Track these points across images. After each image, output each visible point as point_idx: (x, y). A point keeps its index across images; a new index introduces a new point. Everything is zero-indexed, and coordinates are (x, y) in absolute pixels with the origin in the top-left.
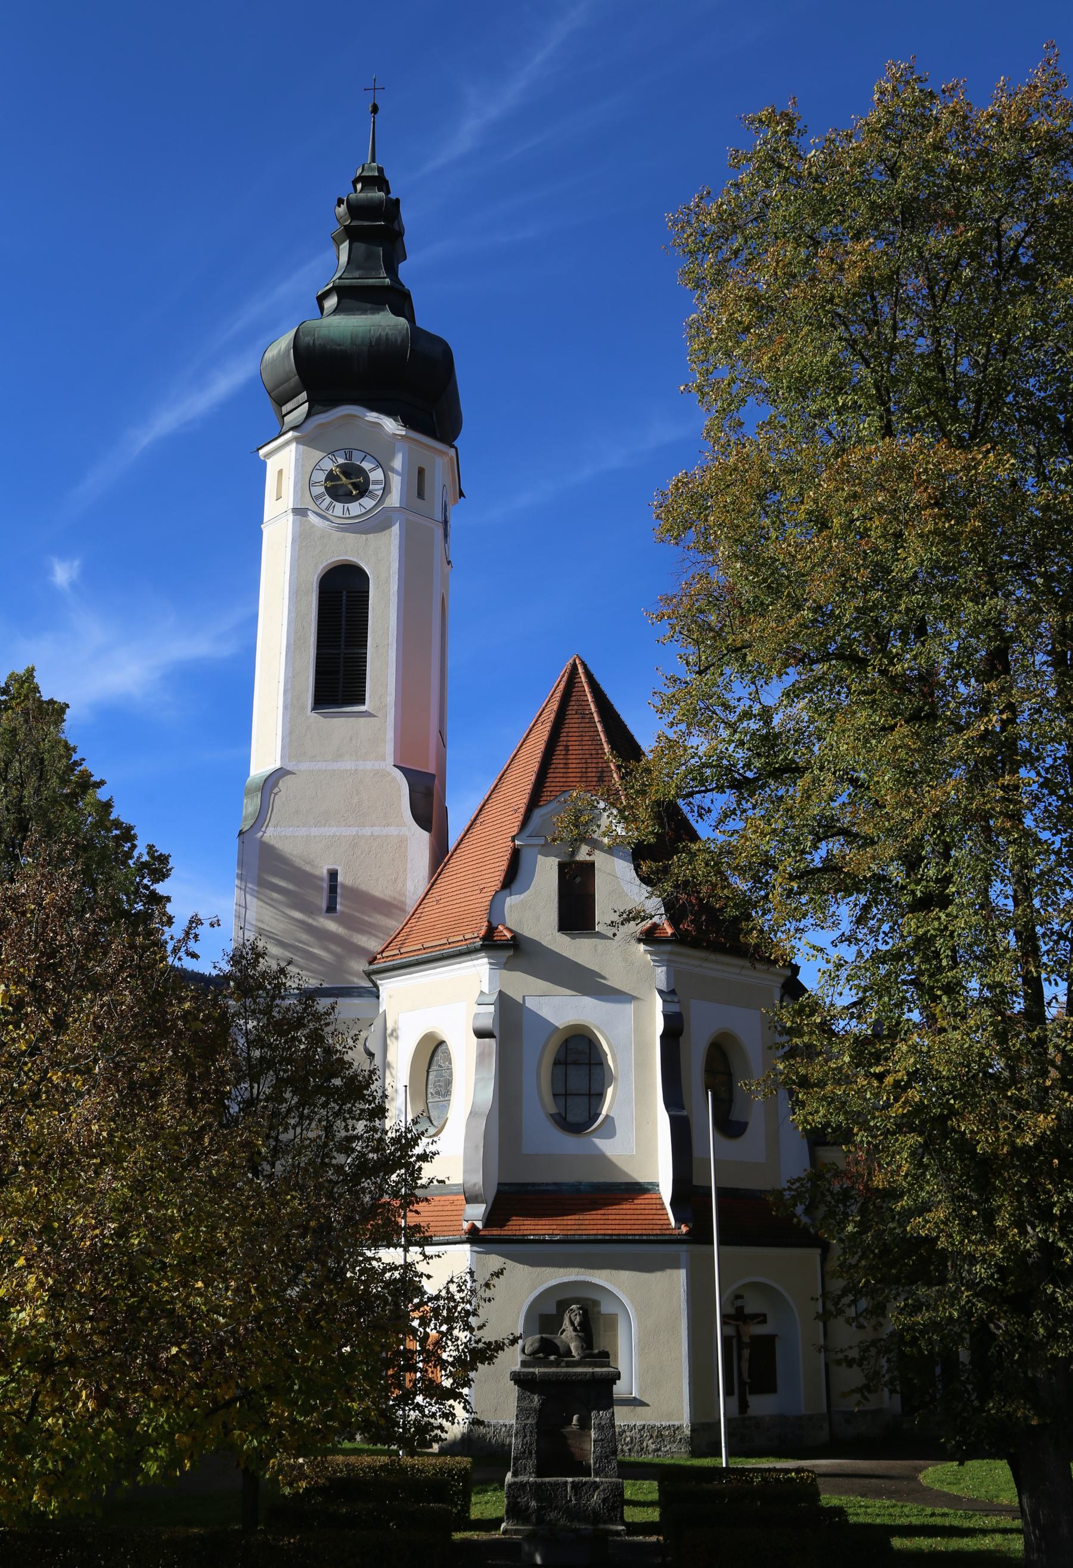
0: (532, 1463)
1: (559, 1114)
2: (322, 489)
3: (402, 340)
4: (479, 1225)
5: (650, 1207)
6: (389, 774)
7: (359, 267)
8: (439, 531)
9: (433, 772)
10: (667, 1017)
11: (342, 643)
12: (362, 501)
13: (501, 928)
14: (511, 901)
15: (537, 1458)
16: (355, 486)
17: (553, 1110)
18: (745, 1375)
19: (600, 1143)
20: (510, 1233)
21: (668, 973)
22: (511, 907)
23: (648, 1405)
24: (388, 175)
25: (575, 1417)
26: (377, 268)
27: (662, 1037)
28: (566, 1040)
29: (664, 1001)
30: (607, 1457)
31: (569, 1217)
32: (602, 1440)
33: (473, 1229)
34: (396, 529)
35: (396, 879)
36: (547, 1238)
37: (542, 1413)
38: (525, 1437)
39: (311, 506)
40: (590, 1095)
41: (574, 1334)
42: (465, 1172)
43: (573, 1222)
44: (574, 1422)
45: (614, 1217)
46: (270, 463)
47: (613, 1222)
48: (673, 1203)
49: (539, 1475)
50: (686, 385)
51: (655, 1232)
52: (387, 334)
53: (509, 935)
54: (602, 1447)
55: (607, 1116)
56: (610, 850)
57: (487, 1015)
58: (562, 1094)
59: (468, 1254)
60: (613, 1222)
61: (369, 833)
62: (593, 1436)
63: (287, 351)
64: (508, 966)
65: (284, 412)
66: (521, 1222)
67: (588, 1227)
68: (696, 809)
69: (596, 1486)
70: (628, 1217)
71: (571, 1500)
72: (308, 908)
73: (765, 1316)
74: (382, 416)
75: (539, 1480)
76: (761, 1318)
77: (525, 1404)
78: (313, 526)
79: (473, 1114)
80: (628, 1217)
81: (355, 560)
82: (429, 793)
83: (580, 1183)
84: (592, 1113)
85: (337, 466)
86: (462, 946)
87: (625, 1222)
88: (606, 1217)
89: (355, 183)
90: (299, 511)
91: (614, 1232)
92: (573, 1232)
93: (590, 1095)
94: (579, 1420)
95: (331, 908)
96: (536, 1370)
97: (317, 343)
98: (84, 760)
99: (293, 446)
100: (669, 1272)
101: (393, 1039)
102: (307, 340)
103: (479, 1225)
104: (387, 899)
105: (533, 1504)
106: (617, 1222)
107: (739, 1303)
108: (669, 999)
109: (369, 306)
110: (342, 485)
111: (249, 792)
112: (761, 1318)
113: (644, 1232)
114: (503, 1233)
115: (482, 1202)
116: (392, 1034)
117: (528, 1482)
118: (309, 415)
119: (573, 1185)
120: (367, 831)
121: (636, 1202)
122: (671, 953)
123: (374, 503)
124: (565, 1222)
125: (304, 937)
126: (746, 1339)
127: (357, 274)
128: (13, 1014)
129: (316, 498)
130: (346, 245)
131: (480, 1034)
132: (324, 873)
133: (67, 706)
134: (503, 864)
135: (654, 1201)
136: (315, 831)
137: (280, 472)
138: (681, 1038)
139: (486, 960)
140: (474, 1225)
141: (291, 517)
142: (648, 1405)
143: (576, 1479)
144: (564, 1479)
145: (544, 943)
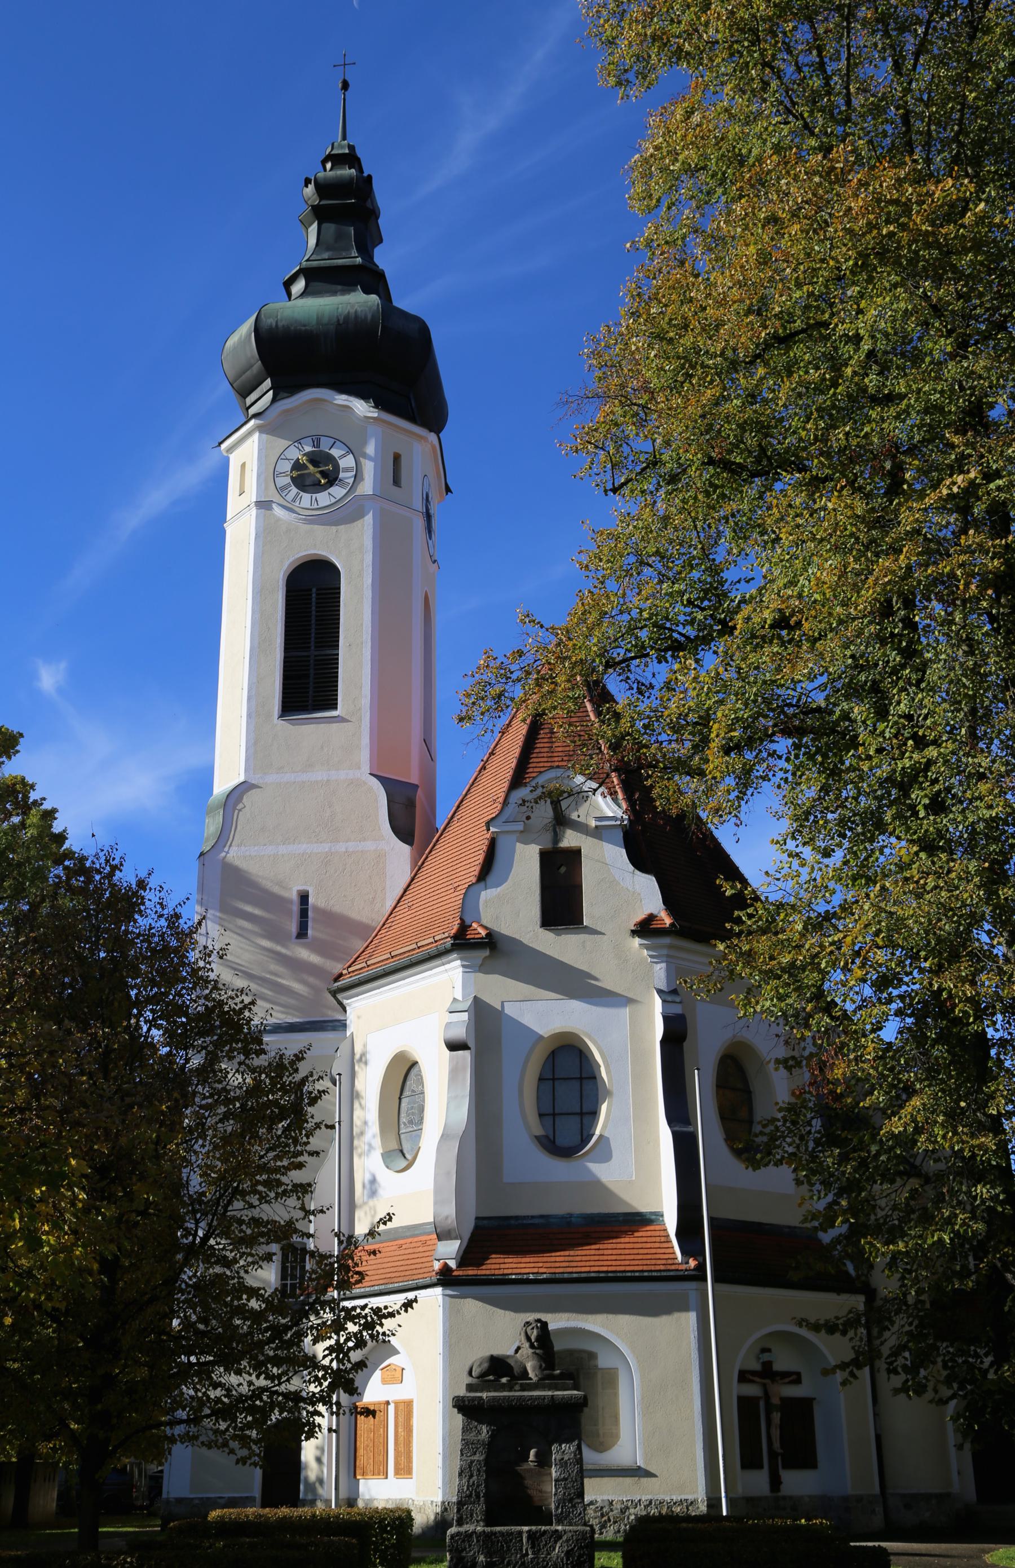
0: (480, 1508)
1: (547, 1137)
2: (288, 480)
3: (373, 316)
4: (452, 1264)
5: (653, 1239)
6: (365, 783)
7: (328, 249)
8: (420, 523)
9: (416, 782)
10: (667, 1019)
11: (312, 644)
12: (332, 490)
13: (475, 925)
14: (486, 895)
15: (486, 1502)
16: (324, 474)
17: (539, 1131)
18: (777, 1445)
19: (595, 1167)
20: (488, 1272)
21: (668, 970)
22: (486, 901)
23: (654, 1476)
24: (359, 153)
25: (533, 1452)
26: (348, 249)
27: (662, 1042)
28: (553, 1052)
29: (664, 1001)
30: (571, 1500)
31: (558, 1254)
32: (565, 1479)
33: (446, 1270)
34: (369, 519)
35: (374, 898)
36: (531, 1277)
37: (492, 1447)
38: (471, 1476)
39: (277, 498)
40: (581, 1114)
41: (531, 1351)
42: (435, 1203)
43: (562, 1259)
44: (532, 1457)
45: (610, 1252)
46: (233, 457)
47: (609, 1258)
48: (678, 1234)
49: (488, 1524)
50: (633, 242)
51: (658, 1268)
52: (356, 312)
53: (483, 933)
54: (565, 1488)
55: (601, 1136)
56: (598, 833)
57: (460, 1026)
58: (548, 1114)
59: (440, 1298)
60: (609, 1258)
61: (344, 850)
62: (554, 1475)
63: (249, 336)
64: (483, 968)
65: (248, 405)
66: (502, 1261)
67: (580, 1264)
68: (635, 686)
69: (557, 1536)
70: (627, 1252)
71: (527, 1554)
72: (273, 933)
73: (799, 1374)
74: (351, 399)
75: (488, 1529)
76: (794, 1377)
77: (472, 1436)
78: (279, 520)
79: (445, 1137)
80: (627, 1252)
81: (324, 553)
82: (411, 804)
83: (571, 1215)
84: (584, 1136)
85: (304, 455)
86: (432, 949)
87: (623, 1257)
88: (601, 1252)
89: (324, 162)
90: (263, 505)
91: (610, 1269)
92: (561, 1270)
93: (581, 1114)
94: (537, 1455)
95: (302, 933)
96: (485, 1395)
97: (280, 324)
98: (44, 799)
99: (256, 436)
100: (676, 1315)
101: (363, 1065)
102: (268, 322)
103: (452, 1264)
104: (364, 920)
105: (481, 1558)
106: (614, 1257)
107: (766, 1357)
108: (669, 999)
109: (339, 287)
110: (310, 474)
111: (211, 811)
112: (794, 1377)
113: (645, 1268)
114: (479, 1272)
115: (456, 1238)
116: (360, 1060)
117: (474, 1532)
118: (274, 400)
119: (562, 1217)
120: (341, 847)
121: (636, 1234)
122: (670, 947)
123: (345, 491)
124: (553, 1259)
125: (274, 967)
126: (775, 1401)
127: (326, 255)
128: (305, 1409)
129: (281, 490)
130: (314, 228)
131: (453, 1046)
132: (294, 896)
133: (21, 735)
134: (479, 858)
135: (657, 1233)
136: (283, 850)
137: (243, 466)
138: (685, 1044)
139: (458, 963)
140: (446, 1264)
141: (254, 511)
142: (654, 1476)
143: (534, 1528)
144: (518, 1528)
145: (525, 941)
